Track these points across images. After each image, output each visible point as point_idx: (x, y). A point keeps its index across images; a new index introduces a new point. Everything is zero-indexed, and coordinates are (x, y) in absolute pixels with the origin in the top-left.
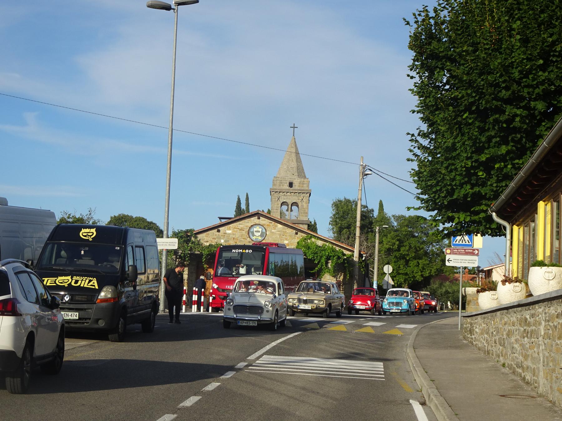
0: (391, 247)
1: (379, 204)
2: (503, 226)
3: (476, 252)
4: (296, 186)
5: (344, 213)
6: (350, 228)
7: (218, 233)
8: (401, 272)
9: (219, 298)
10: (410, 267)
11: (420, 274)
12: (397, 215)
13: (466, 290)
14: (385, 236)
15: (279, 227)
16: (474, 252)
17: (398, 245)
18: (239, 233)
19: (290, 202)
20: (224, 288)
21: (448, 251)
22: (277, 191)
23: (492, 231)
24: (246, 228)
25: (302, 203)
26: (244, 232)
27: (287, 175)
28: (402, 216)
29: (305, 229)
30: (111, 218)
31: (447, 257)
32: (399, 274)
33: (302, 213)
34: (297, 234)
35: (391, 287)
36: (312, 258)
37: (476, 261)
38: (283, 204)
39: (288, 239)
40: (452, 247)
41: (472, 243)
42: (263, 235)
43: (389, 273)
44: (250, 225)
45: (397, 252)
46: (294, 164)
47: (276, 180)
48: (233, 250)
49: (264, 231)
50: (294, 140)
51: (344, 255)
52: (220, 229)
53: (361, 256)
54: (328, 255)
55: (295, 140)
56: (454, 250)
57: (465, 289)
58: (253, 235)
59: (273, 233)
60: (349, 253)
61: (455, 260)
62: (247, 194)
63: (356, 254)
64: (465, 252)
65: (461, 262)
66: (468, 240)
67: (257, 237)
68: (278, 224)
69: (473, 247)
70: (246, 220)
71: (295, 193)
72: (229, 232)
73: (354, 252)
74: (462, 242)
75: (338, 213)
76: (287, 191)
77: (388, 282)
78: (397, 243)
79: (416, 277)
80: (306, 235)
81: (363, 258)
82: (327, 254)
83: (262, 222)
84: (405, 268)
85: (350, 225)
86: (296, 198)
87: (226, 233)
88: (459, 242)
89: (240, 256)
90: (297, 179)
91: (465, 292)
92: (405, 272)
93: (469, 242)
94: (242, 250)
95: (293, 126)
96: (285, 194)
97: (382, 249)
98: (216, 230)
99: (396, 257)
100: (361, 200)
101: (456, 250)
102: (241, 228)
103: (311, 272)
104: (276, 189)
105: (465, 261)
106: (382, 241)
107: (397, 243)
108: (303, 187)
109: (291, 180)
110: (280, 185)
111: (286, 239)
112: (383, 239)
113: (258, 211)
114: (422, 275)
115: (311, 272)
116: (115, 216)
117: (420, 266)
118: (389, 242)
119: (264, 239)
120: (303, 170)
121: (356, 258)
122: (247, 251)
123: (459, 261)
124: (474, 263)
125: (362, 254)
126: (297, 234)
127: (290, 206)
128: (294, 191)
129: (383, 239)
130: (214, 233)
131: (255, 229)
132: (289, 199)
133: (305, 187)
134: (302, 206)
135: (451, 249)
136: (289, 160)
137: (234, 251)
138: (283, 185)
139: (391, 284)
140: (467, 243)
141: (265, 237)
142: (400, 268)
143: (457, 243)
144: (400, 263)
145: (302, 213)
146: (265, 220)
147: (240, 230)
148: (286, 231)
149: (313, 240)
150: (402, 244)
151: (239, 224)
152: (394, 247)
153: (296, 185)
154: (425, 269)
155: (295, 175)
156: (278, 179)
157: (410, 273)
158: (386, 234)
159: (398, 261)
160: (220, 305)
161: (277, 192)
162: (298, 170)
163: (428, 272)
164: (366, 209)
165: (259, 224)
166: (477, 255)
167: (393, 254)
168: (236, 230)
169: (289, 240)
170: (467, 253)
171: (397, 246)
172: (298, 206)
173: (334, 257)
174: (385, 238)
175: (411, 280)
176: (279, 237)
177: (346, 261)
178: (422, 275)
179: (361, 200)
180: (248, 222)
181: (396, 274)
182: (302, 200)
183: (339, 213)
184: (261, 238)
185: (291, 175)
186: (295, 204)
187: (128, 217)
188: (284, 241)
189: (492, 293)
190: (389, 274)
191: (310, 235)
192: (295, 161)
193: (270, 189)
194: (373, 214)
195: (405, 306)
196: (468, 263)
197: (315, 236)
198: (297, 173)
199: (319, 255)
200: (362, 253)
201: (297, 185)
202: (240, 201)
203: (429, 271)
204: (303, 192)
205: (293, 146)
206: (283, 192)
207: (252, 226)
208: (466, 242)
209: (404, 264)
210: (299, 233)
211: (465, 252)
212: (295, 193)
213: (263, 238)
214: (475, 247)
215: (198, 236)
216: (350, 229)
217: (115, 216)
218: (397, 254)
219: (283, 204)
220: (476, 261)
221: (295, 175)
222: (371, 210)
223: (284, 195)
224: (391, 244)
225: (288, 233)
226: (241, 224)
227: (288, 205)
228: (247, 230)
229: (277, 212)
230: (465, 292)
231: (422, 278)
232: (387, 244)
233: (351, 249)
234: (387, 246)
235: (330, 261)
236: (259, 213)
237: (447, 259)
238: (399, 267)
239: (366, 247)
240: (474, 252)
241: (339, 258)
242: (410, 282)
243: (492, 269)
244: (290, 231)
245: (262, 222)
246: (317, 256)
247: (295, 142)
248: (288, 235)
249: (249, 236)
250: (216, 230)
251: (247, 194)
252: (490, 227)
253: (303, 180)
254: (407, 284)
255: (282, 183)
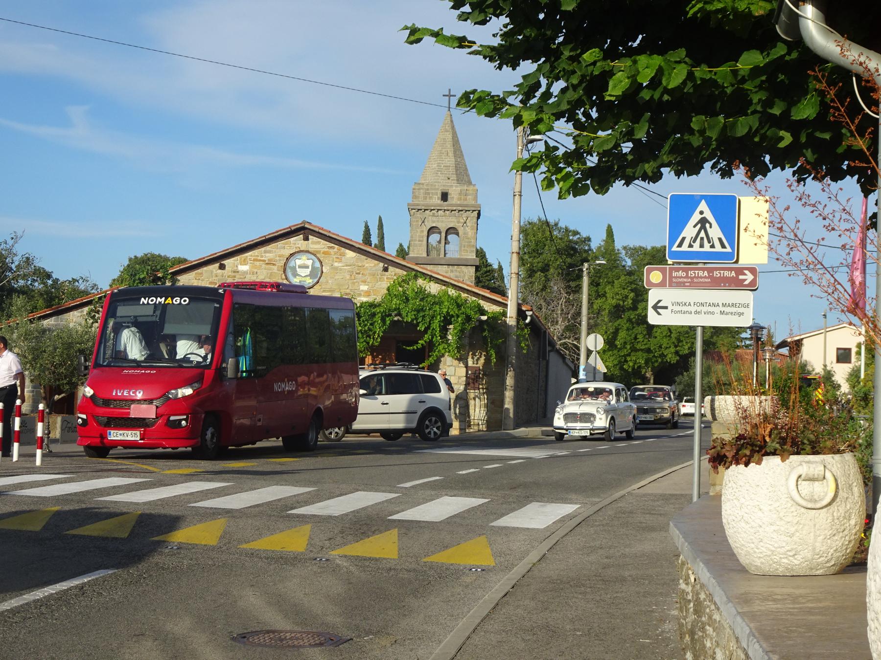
0: (621, 303)
1: (605, 231)
2: (859, 78)
3: (749, 277)
4: (454, 199)
5: (537, 245)
6: (548, 270)
7: (220, 271)
8: (638, 346)
9: (97, 422)
10: (656, 337)
11: (673, 350)
12: (632, 247)
13: (717, 404)
14: (609, 283)
15: (348, 256)
16: (741, 277)
17: (632, 299)
18: (265, 272)
19: (443, 227)
20: (107, 396)
21: (656, 276)
22: (420, 208)
23: (796, 136)
24: (280, 260)
25: (464, 229)
26: (275, 268)
27: (438, 179)
28: (641, 247)
29: (391, 256)
30: (130, 260)
31: (653, 297)
32: (636, 350)
33: (464, 247)
34: (386, 270)
35: (602, 377)
36: (413, 320)
37: (748, 306)
38: (432, 230)
39: (368, 280)
40: (670, 262)
41: (733, 248)
42: (317, 274)
43: (597, 350)
44: (287, 252)
45: (631, 312)
46: (450, 161)
47: (419, 189)
48: (143, 299)
49: (318, 265)
50: (449, 118)
51: (482, 312)
52: (225, 262)
53: (521, 314)
54: (448, 313)
55: (451, 118)
56: (674, 274)
57: (713, 401)
58: (295, 275)
59: (336, 268)
60: (497, 309)
61: (678, 304)
62: (380, 218)
63: (511, 311)
64: (709, 277)
65: (697, 312)
66: (720, 240)
67: (304, 279)
68: (347, 251)
69: (737, 262)
70: (280, 244)
71: (452, 211)
72: (243, 268)
73: (506, 305)
74: (702, 246)
75: (526, 245)
76: (438, 208)
77: (595, 368)
78: (632, 295)
79: (665, 356)
80: (405, 273)
81: (526, 319)
82: (445, 310)
83: (312, 246)
84: (646, 341)
85: (548, 265)
86: (454, 219)
87: (238, 272)
88: (690, 246)
89: (158, 313)
90: (456, 186)
91: (713, 409)
92: (647, 346)
93: (723, 246)
94: (164, 298)
95: (447, 93)
96: (434, 214)
97: (604, 307)
98: (217, 265)
99: (629, 320)
100: (520, 195)
101: (680, 273)
102: (269, 260)
103: (408, 348)
104: (418, 205)
105: (711, 309)
106: (605, 292)
107: (632, 295)
108: (466, 200)
109: (445, 189)
110: (425, 198)
111: (363, 282)
112: (607, 289)
113: (304, 222)
114: (677, 353)
115: (408, 348)
116: (135, 256)
117: (672, 335)
118: (618, 294)
119: (318, 282)
120: (466, 169)
121: (511, 318)
122: (177, 301)
123: (693, 309)
124: (743, 314)
125: (524, 312)
126: (386, 270)
127: (443, 235)
128: (450, 208)
129: (607, 289)
130: (212, 272)
131: (298, 262)
132: (442, 222)
133: (470, 201)
134: (465, 234)
135: (663, 271)
136: (441, 153)
137: (146, 302)
138: (430, 198)
139: (601, 372)
140: (718, 248)
141: (320, 278)
142: (638, 340)
143: (685, 248)
144: (637, 332)
145: (464, 247)
146: (319, 243)
147: (267, 264)
148: (364, 264)
149: (420, 281)
150: (640, 298)
151: (265, 252)
152: (626, 303)
153: (453, 197)
154: (682, 341)
155: (452, 180)
156: (421, 186)
157: (655, 349)
158: (610, 280)
159: (634, 328)
160: (98, 440)
161: (421, 210)
162: (457, 170)
163: (686, 347)
164: (578, 236)
165: (308, 252)
166: (752, 287)
167: (624, 315)
168: (258, 263)
169: (370, 284)
170: (717, 283)
171: (631, 302)
172: (457, 234)
173: (458, 316)
174: (610, 287)
175: (657, 361)
176: (348, 277)
177: (485, 327)
178: (677, 353)
179: (520, 195)
180: (284, 248)
181: (630, 351)
182: (465, 223)
183: (528, 244)
184: (311, 281)
185: (445, 180)
186: (451, 230)
187: (159, 258)
188: (359, 286)
189: (804, 470)
190: (598, 352)
191: (414, 273)
192: (451, 154)
193: (409, 204)
194: (589, 246)
195: (602, 422)
196: (722, 313)
197: (424, 274)
198: (455, 176)
199: (427, 313)
200: (524, 309)
201: (455, 197)
202: (369, 230)
203: (689, 345)
204: (466, 209)
205: (448, 128)
206: (431, 210)
207: (292, 255)
208: (713, 246)
209: (645, 333)
210: (391, 269)
211: (709, 277)
212: (452, 211)
213: (316, 280)
214: (744, 260)
215: (179, 278)
216: (547, 273)
217: (135, 256)
218: (632, 315)
219: (432, 230)
220: (748, 306)
221: (452, 180)
222: (585, 238)
223: (434, 215)
224: (621, 298)
225: (367, 268)
226: (270, 252)
227: (440, 233)
228: (283, 263)
229: (421, 245)
230: (713, 409)
231: (678, 358)
232: (613, 298)
233: (500, 300)
234: (614, 302)
235: (451, 327)
236: (307, 229)
237: (651, 302)
238: (636, 338)
239: (566, 302)
240: (741, 277)
241: (468, 319)
242: (656, 365)
243: (802, 339)
244: (373, 265)
245: (312, 246)
246: (424, 316)
247: (452, 121)
248: (366, 272)
249: (286, 276)
250: (217, 265)
251: (380, 218)
252: (786, 114)
253: (465, 187)
254: (650, 369)
255: (429, 194)
